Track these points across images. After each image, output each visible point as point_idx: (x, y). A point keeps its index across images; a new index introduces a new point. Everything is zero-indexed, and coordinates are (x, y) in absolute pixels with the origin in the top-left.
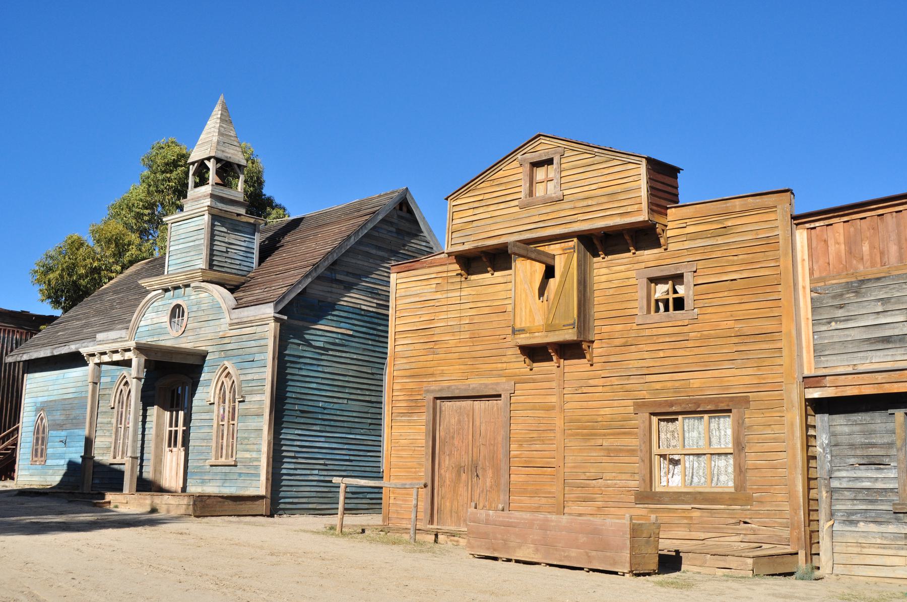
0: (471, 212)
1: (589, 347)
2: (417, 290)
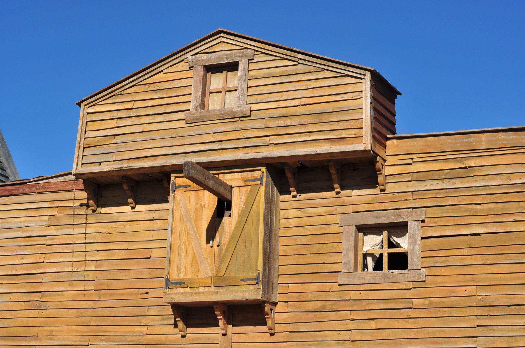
0: (113, 124)
1: (271, 310)
2: (20, 222)
